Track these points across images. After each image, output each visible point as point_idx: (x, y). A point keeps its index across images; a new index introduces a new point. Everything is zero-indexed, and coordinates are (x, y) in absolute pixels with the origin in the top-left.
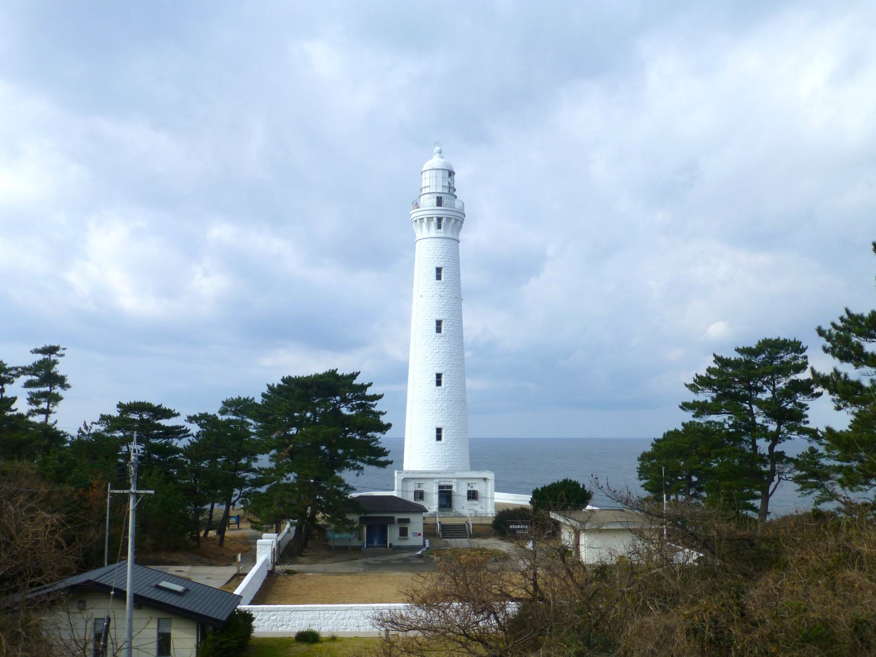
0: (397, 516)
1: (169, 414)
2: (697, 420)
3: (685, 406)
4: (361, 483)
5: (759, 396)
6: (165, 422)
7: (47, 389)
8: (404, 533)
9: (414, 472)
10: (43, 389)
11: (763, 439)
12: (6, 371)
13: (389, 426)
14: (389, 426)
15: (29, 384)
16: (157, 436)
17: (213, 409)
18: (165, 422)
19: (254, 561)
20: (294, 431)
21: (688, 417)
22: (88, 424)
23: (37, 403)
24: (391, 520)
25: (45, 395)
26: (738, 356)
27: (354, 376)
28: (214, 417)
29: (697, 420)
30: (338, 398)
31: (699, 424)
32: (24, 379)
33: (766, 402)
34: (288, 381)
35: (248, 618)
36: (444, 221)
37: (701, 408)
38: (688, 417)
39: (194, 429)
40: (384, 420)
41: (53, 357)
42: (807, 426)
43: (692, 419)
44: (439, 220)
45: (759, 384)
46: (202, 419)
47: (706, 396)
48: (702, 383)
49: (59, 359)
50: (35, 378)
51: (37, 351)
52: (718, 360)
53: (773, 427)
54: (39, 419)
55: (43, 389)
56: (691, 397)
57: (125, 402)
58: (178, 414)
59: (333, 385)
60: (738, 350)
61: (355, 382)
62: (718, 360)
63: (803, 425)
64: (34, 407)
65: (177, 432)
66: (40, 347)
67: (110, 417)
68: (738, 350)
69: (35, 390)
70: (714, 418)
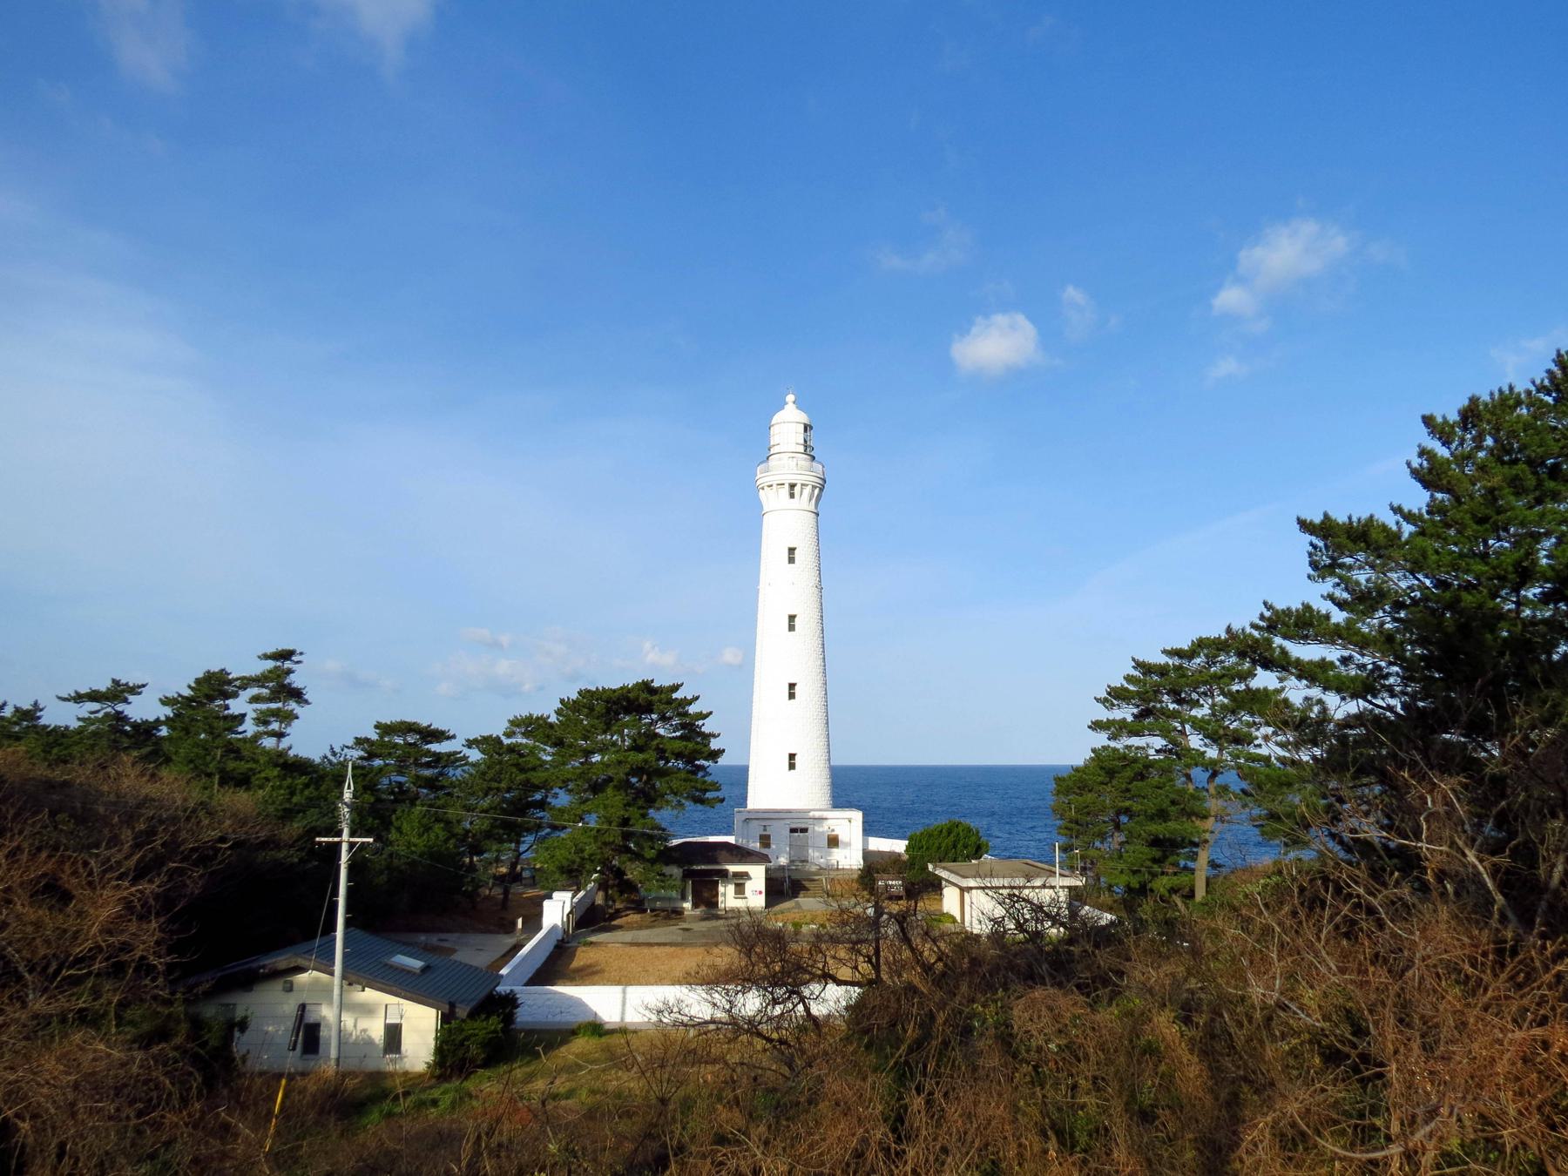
0: (733, 868)
1: (439, 736)
2: (1113, 744)
3: (1097, 726)
4: (684, 827)
5: (1193, 713)
6: (435, 747)
7: (280, 705)
8: (740, 890)
9: (757, 811)
10: (273, 706)
11: (1199, 769)
12: (230, 682)
13: (720, 752)
14: (720, 752)
15: (255, 699)
16: (428, 765)
17: (497, 728)
18: (435, 747)
19: (540, 928)
20: (596, 758)
21: (1101, 739)
22: (337, 750)
23: (266, 723)
24: (724, 874)
25: (276, 714)
26: (1163, 660)
27: (675, 688)
28: (498, 740)
29: (1113, 744)
30: (654, 716)
31: (1115, 750)
32: (254, 691)
33: (1202, 720)
34: (585, 694)
35: (510, 1001)
36: (797, 490)
37: (1116, 729)
38: (1101, 739)
39: (475, 755)
40: (714, 745)
41: (287, 665)
42: (1258, 751)
43: (1107, 743)
44: (792, 486)
45: (1195, 696)
46: (487, 743)
47: (1126, 713)
48: (1117, 695)
49: (294, 667)
50: (265, 691)
51: (266, 657)
52: (1139, 665)
53: (1212, 753)
54: (269, 743)
55: (273, 706)
56: (1104, 714)
57: (386, 720)
58: (454, 737)
59: (643, 700)
60: (1164, 652)
61: (674, 696)
62: (1139, 665)
63: (1252, 750)
64: (262, 729)
65: (452, 759)
66: (271, 650)
67: (367, 740)
68: (1164, 652)
69: (263, 706)
70: (1136, 741)
